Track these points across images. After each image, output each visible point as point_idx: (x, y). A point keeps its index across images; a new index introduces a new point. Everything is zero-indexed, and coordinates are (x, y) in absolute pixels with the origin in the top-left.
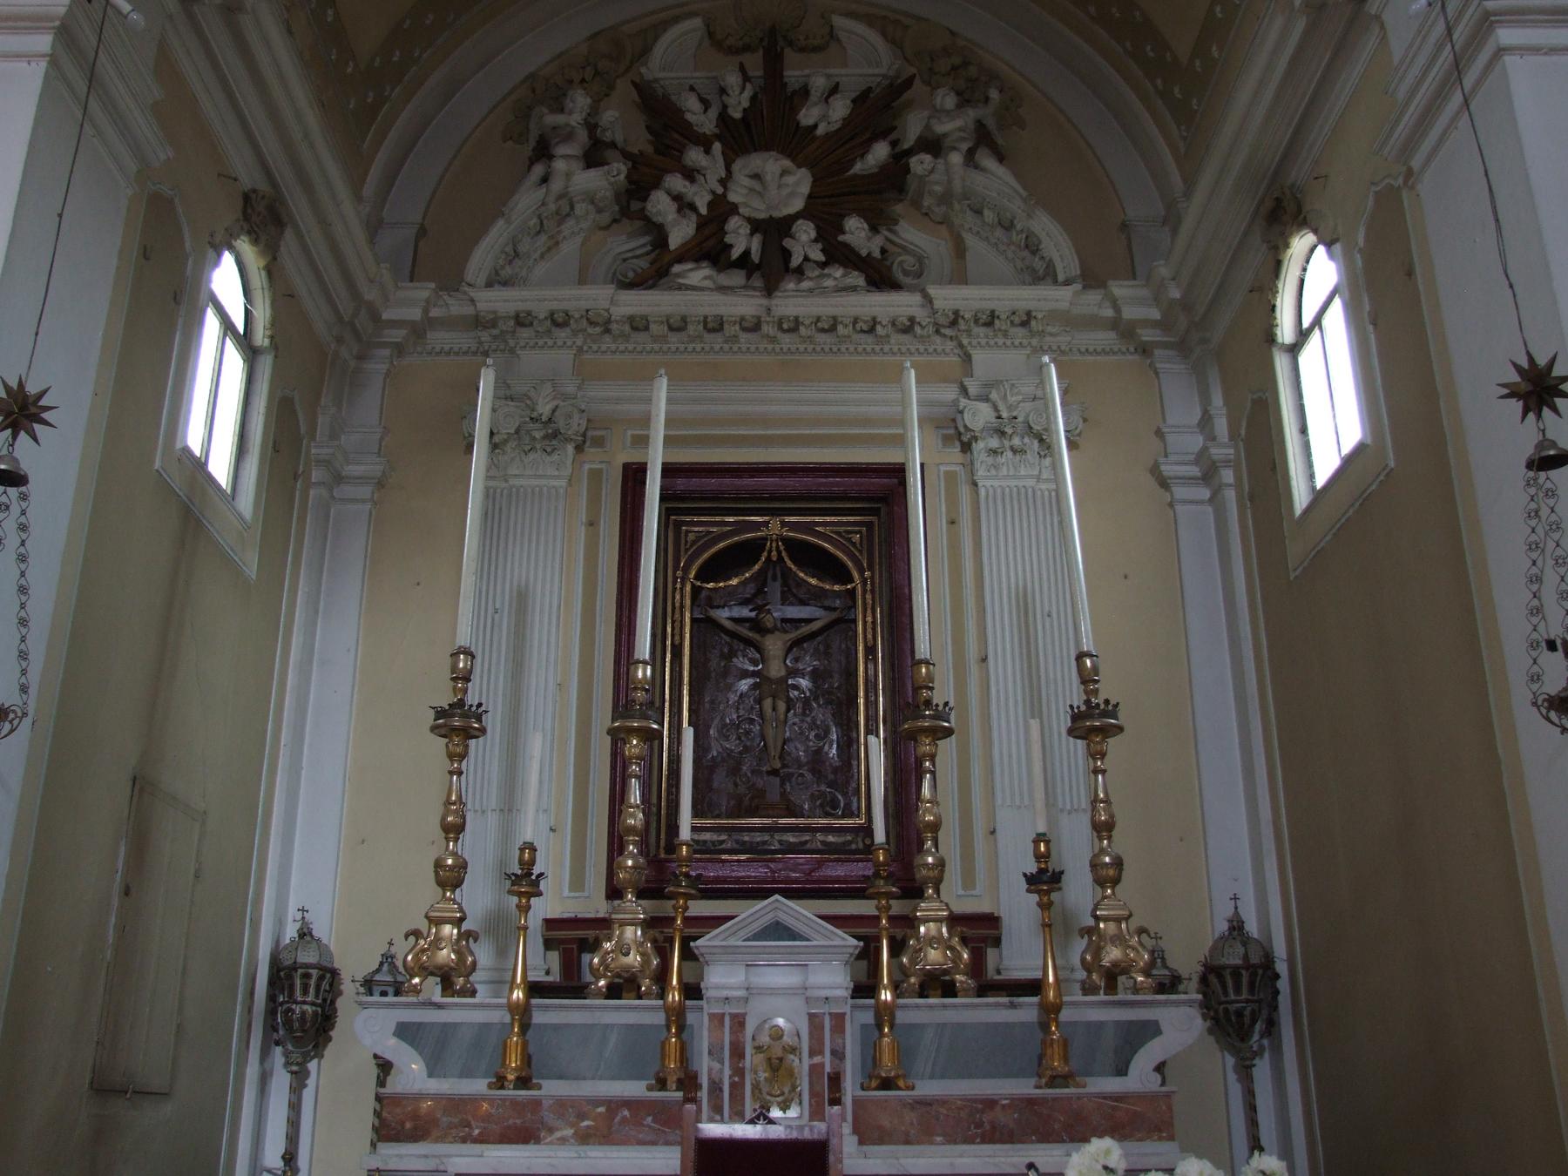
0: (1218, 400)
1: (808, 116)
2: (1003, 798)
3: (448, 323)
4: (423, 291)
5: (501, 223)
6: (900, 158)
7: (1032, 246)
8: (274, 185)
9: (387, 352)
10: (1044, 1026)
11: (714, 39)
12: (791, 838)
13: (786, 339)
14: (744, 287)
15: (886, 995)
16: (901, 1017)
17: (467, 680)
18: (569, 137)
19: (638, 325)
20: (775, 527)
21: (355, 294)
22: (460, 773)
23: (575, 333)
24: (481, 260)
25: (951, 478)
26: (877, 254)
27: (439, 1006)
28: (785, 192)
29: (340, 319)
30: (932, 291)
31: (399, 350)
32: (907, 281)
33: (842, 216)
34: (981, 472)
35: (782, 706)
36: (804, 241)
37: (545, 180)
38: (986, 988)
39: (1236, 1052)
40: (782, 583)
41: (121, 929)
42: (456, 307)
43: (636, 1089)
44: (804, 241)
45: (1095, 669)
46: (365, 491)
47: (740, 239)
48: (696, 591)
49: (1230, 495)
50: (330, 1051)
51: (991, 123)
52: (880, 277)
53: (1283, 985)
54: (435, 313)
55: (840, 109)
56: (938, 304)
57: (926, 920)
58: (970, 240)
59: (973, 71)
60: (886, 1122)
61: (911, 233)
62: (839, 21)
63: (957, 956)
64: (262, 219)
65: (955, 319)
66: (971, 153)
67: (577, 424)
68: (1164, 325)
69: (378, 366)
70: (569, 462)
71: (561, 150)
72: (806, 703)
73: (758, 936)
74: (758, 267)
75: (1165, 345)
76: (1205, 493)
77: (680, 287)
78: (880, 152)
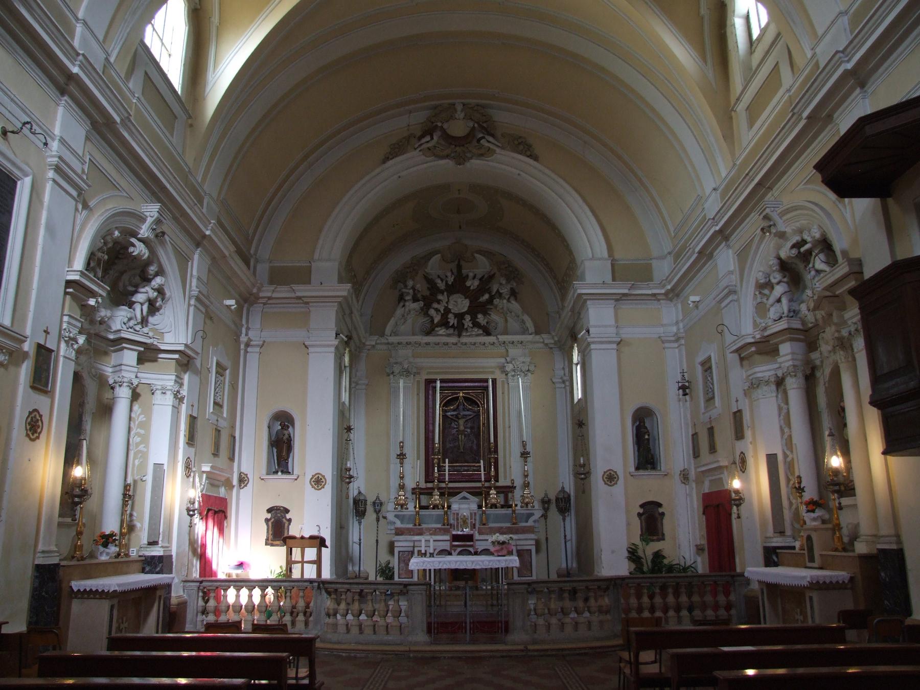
1: (468, 284)
3: (381, 344)
4: (376, 338)
6: (492, 298)
7: (523, 322)
11: (443, 259)
13: (464, 347)
18: (408, 294)
21: (360, 340)
24: (388, 330)
25: (503, 382)
42: (383, 340)
43: (439, 526)
46: (364, 387)
47: (452, 320)
52: (487, 333)
61: (494, 317)
65: (504, 343)
67: (415, 370)
68: (555, 343)
69: (364, 355)
71: (407, 298)
78: (486, 296)
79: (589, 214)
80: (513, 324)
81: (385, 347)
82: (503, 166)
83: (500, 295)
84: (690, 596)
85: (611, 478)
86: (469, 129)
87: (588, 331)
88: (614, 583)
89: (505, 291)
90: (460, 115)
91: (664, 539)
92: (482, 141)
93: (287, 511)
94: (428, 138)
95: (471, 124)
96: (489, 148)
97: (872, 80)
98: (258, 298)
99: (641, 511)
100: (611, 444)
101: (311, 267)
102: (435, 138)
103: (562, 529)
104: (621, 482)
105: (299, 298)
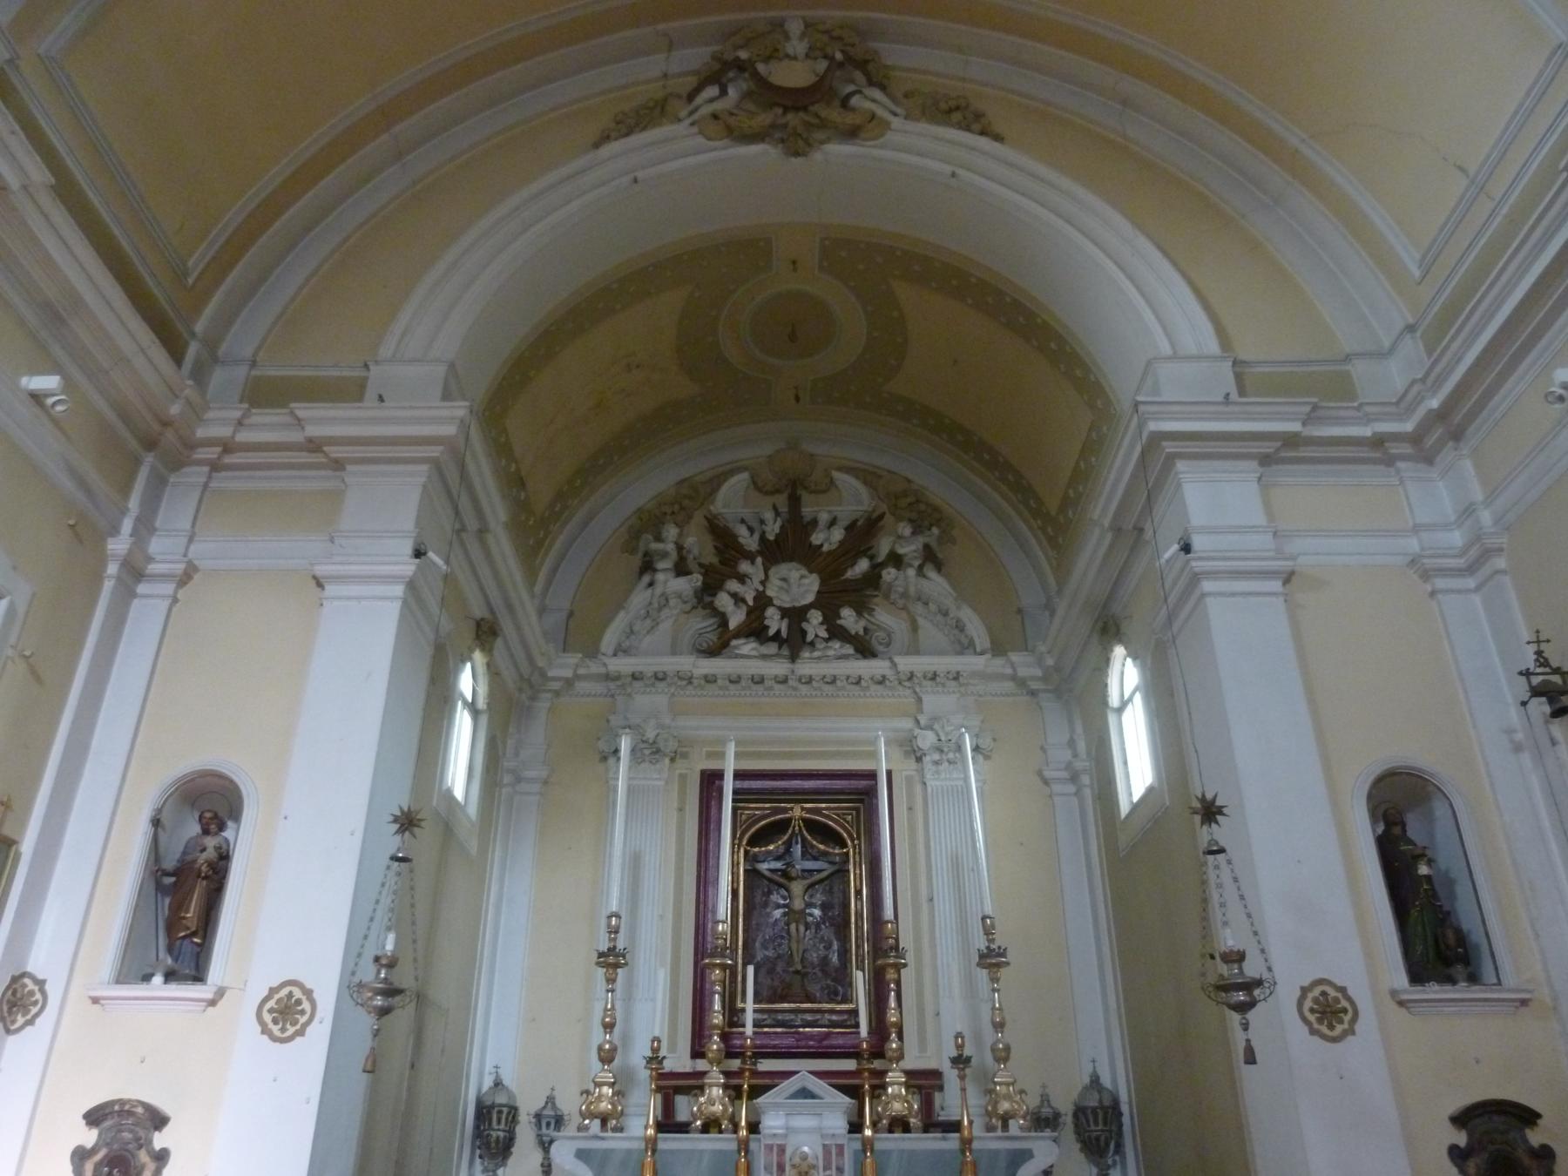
0: (1079, 729)
1: (817, 538)
2: (939, 1008)
4: (573, 659)
5: (622, 614)
6: (876, 568)
7: (960, 626)
8: (492, 611)
9: (549, 695)
10: (963, 1152)
11: (756, 485)
12: (809, 1017)
13: (804, 689)
14: (776, 655)
15: (868, 1132)
16: (878, 1146)
17: (616, 932)
18: (664, 555)
19: (710, 679)
20: (797, 812)
21: (531, 659)
22: (613, 991)
23: (670, 685)
24: (609, 639)
25: (909, 780)
26: (861, 632)
27: (603, 1139)
28: (802, 589)
29: (521, 676)
30: (897, 659)
31: (557, 693)
32: (881, 648)
34: (928, 776)
35: (802, 928)
36: (814, 624)
37: (651, 584)
38: (931, 1124)
39: (1097, 1165)
40: (804, 843)
41: (409, 1089)
42: (594, 668)
44: (814, 624)
45: (993, 926)
47: (774, 622)
48: (746, 852)
49: (1087, 792)
50: (511, 1161)
51: (934, 544)
52: (864, 649)
53: (1126, 1120)
54: (581, 671)
55: (837, 535)
56: (901, 668)
57: (892, 1084)
58: (921, 621)
61: (885, 617)
62: (836, 475)
63: (910, 1107)
64: (485, 633)
66: (920, 568)
67: (672, 745)
68: (1045, 679)
69: (543, 704)
71: (661, 565)
72: (818, 925)
73: (811, 1072)
74: (786, 641)
75: (1045, 691)
76: (1072, 789)
77: (738, 656)
78: (863, 565)
81: (599, 688)
82: (902, 171)
83: (896, 560)
85: (1329, 1011)
87: (1186, 548)
89: (910, 549)
90: (798, 47)
92: (854, 101)
93: (158, 1120)
94: (712, 91)
96: (873, 116)
97: (1471, 429)
98: (191, 445)
99: (1461, 1139)
101: (366, 379)
102: (732, 92)
104: (1367, 1023)
105: (314, 446)
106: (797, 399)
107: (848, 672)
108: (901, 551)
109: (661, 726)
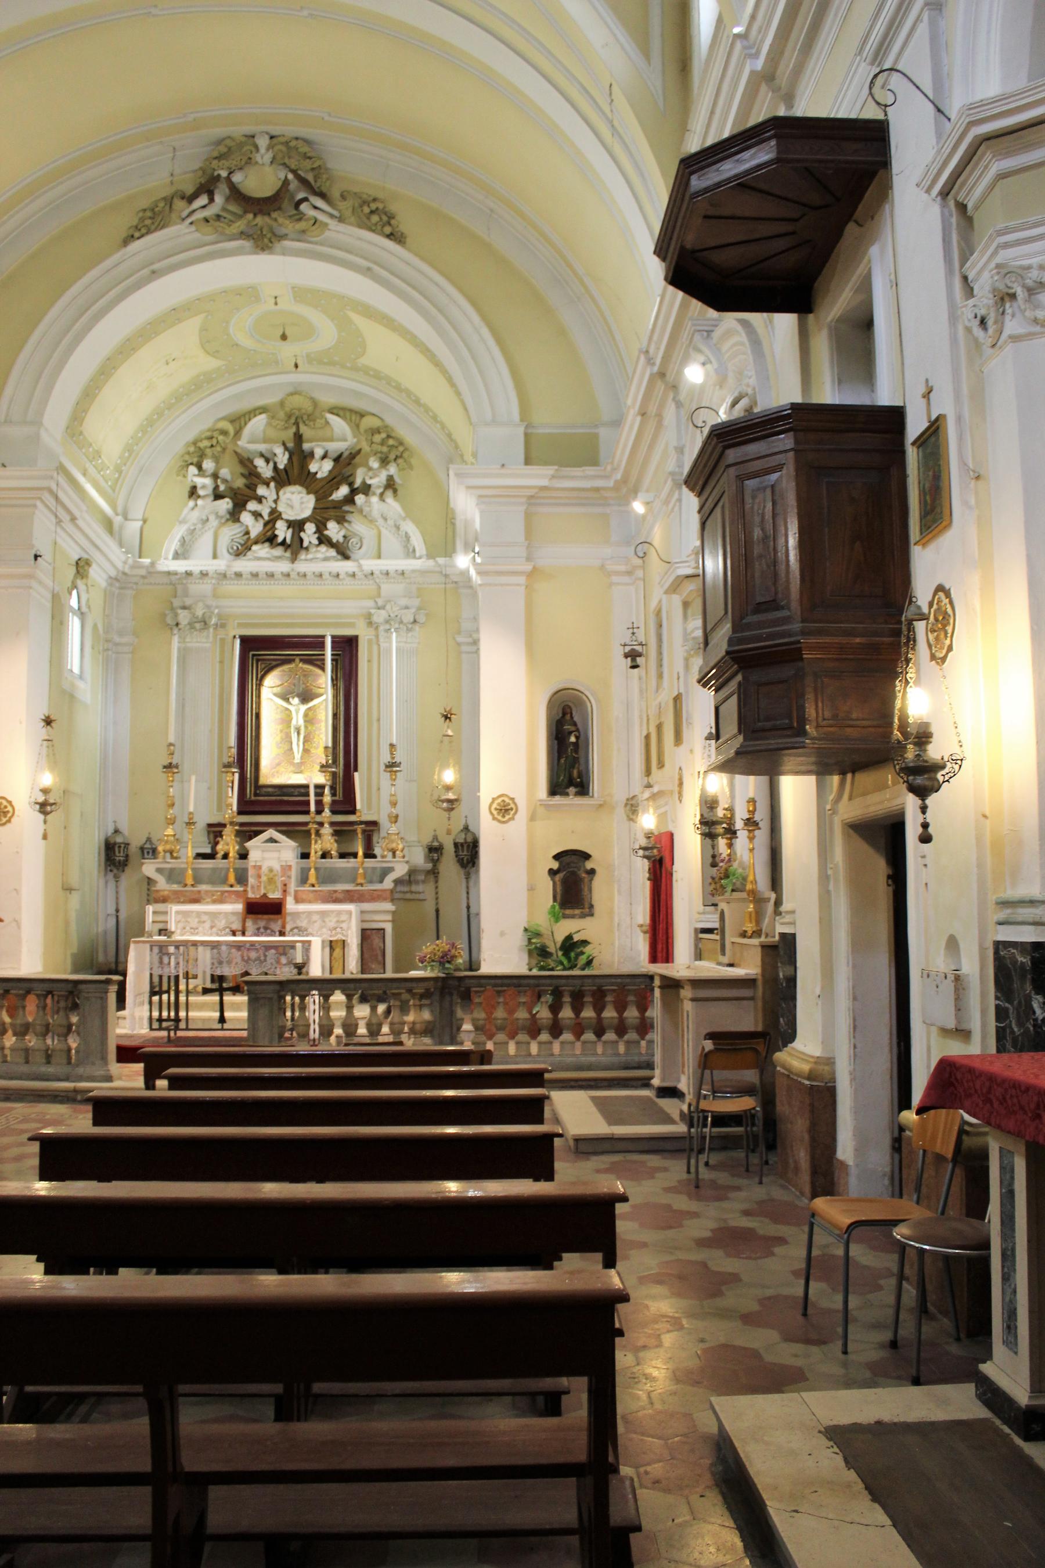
7: (407, 537)
25: (370, 641)
26: (341, 540)
30: (362, 562)
33: (328, 520)
34: (381, 640)
36: (309, 533)
44: (309, 533)
47: (282, 531)
52: (343, 553)
55: (327, 466)
58: (384, 531)
59: (391, 442)
60: (304, 897)
61: (358, 526)
66: (382, 495)
70: (211, 635)
71: (201, 492)
78: (344, 491)
79: (491, 342)
80: (391, 542)
83: (366, 489)
84: (577, 1010)
86: (280, 183)
88: (506, 984)
89: (377, 481)
90: (264, 156)
91: (592, 915)
92: (303, 207)
94: (203, 200)
95: (282, 174)
99: (555, 865)
100: (508, 757)
102: (219, 199)
103: (465, 895)
104: (522, 815)
106: (296, 366)
107: (330, 570)
108: (369, 482)
109: (208, 607)
